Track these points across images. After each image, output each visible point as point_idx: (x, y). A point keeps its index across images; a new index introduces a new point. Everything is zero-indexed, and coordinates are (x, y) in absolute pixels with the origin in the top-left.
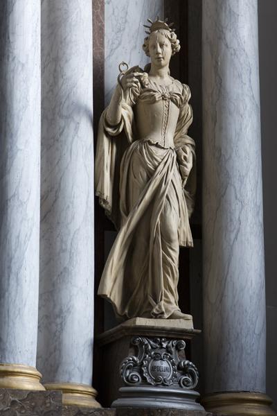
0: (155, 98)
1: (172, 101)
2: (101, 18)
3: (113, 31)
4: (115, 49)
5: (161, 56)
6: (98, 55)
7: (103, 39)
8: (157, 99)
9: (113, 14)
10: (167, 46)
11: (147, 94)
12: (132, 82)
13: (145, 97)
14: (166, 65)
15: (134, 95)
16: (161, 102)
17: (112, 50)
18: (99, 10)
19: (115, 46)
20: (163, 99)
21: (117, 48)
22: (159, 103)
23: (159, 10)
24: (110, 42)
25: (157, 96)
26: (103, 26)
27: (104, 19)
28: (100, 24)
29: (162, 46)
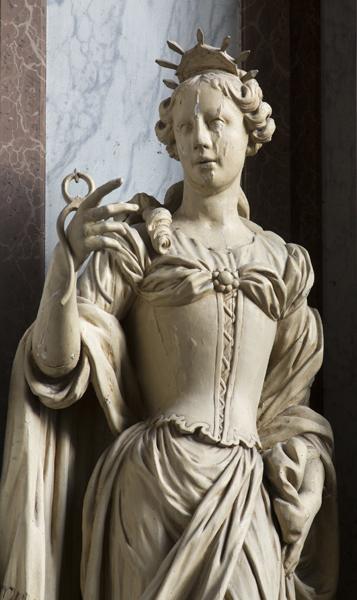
1: (248, 294)
3: (74, 87)
4: (82, 142)
5: (209, 154)
6: (24, 163)
7: (42, 110)
8: (196, 291)
10: (228, 122)
12: (105, 232)
13: (160, 284)
14: (229, 183)
15: (125, 279)
16: (211, 298)
18: (28, 24)
19: (79, 134)
20: (217, 289)
21: (88, 137)
22: (203, 302)
23: (223, 20)
24: (65, 124)
25: (198, 279)
26: (42, 71)
27: (42, 47)
28: (29, 67)
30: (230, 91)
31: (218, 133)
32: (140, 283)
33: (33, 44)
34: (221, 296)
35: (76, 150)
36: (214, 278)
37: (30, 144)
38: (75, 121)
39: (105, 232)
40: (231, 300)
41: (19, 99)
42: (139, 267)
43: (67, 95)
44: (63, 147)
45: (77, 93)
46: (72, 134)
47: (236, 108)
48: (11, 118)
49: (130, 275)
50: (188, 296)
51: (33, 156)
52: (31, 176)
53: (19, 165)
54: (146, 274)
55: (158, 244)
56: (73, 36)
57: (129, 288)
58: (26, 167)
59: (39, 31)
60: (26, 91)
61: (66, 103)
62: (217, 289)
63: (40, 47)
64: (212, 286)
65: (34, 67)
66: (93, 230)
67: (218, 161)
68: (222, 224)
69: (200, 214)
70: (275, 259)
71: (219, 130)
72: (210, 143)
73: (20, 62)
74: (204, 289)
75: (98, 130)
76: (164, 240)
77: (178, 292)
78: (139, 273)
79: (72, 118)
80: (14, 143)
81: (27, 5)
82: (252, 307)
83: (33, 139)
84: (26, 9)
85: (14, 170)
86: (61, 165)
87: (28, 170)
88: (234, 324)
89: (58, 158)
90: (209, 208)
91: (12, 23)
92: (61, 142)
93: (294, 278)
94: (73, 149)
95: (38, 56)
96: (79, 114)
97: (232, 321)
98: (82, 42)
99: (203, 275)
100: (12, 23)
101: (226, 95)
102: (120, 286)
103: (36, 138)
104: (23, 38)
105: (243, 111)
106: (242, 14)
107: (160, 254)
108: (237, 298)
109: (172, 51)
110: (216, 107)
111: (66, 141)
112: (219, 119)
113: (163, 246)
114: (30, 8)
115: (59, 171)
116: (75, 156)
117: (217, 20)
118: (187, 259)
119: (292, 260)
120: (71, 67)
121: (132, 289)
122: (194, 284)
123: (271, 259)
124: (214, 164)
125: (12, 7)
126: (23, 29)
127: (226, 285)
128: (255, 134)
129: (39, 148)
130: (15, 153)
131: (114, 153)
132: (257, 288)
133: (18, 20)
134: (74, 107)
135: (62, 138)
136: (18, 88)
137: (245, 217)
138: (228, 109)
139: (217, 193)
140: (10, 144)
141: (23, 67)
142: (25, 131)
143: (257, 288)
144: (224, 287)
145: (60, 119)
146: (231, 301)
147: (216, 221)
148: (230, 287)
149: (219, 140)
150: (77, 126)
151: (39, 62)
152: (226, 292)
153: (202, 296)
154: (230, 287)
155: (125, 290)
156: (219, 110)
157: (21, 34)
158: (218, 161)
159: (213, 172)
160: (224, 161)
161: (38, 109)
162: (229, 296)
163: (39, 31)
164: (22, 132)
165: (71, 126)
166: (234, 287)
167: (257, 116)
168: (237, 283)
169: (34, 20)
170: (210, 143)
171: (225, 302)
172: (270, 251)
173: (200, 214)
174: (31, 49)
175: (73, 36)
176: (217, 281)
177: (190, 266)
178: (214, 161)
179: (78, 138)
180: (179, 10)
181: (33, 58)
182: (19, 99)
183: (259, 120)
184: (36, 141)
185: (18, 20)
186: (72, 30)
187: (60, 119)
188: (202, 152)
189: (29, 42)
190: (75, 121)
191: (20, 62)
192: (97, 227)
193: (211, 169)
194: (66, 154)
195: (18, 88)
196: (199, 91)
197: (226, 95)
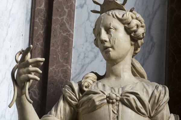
0: (94, 100)
1: (124, 103)
2: (68, 26)
3: (86, 41)
4: (89, 64)
5: (107, 44)
6: (60, 74)
7: (70, 52)
8: (97, 103)
9: (88, 19)
10: (116, 29)
11: (85, 98)
12: (30, 72)
13: (83, 103)
14: (123, 58)
15: (70, 104)
16: (106, 106)
17: (83, 66)
18: (65, 17)
19: (88, 60)
20: (108, 102)
21: (92, 61)
22: (102, 109)
23: (159, 6)
24: (81, 57)
25: (97, 99)
26: (72, 36)
27: (72, 26)
28: (65, 34)
29: (108, 30)
30: (116, 15)
31: (111, 34)
32: (77, 106)
33: (67, 25)
34: (111, 105)
35: (86, 67)
36: (107, 97)
37: (63, 66)
38: (86, 55)
39: (30, 72)
40: (116, 107)
41: (59, 48)
42: (76, 99)
43: (83, 45)
44: (81, 66)
45: (88, 44)
46: (85, 61)
47: (120, 23)
48: (55, 56)
49: (71, 102)
50: (94, 107)
51: (64, 71)
52: (63, 80)
53: (57, 75)
54: (79, 100)
55: (83, 86)
56: (87, 20)
57: (72, 108)
58: (60, 76)
59: (70, 19)
60: (63, 44)
61: (83, 48)
62: (108, 102)
63: (70, 26)
64: (106, 101)
65: (67, 34)
66: (23, 72)
67: (112, 47)
68: (121, 77)
69: (110, 74)
70: (147, 90)
71: (112, 33)
72: (108, 40)
73: (60, 33)
74: (102, 102)
75: (97, 58)
76: (86, 84)
77: (90, 105)
78: (76, 101)
79: (85, 54)
80: (56, 67)
81: (65, 9)
82: (130, 111)
83: (64, 64)
84: (65, 11)
85: (55, 78)
86: (79, 74)
87: (62, 77)
88: (117, 117)
89: (78, 71)
90: (114, 71)
91: (58, 17)
92: (79, 65)
93: (154, 97)
94: (85, 67)
95: (69, 29)
96: (88, 52)
97: (116, 116)
98: (91, 22)
99: (101, 96)
100: (58, 17)
101: (114, 17)
102: (68, 108)
103: (66, 63)
104: (62, 23)
105: (124, 24)
106: (168, 2)
107: (85, 91)
108: (118, 105)
109: (96, 4)
110: (109, 23)
111: (81, 64)
112: (111, 28)
113: (86, 87)
114: (67, 10)
115: (77, 77)
116: (85, 70)
117: (156, 6)
118: (94, 90)
119: (155, 91)
120: (86, 33)
121: (74, 108)
122: (96, 100)
123: (145, 90)
124: (111, 49)
125: (58, 11)
126: (63, 19)
127: (112, 99)
128: (132, 35)
129: (67, 68)
130: (56, 71)
131: (38, 40)
132: (127, 100)
133: (60, 16)
134: (86, 49)
135: (80, 63)
136: (59, 44)
137: (144, 78)
138: (115, 23)
139: (117, 63)
140: (54, 67)
141: (62, 35)
142: (61, 61)
143: (127, 100)
144: (111, 101)
145: (79, 55)
146: (116, 107)
147: (118, 76)
148: (115, 101)
149: (112, 37)
150: (87, 57)
151: (69, 32)
152: (113, 103)
153: (101, 106)
154: (115, 101)
155: (71, 109)
156: (110, 24)
157: (61, 21)
158: (112, 47)
159: (110, 53)
160: (115, 47)
161: (68, 51)
162: (114, 105)
163: (70, 19)
164: (60, 61)
165: (84, 57)
166: (117, 101)
167: (129, 25)
168: (118, 99)
169: (68, 15)
170: (108, 40)
171: (113, 107)
172: (145, 87)
173: (110, 74)
174: (66, 27)
175: (87, 20)
176: (108, 99)
177: (95, 93)
178: (111, 48)
179: (88, 62)
180: (138, 4)
181: (67, 31)
182: (59, 48)
183: (131, 27)
184: (66, 65)
185: (60, 16)
186: (87, 17)
187: (79, 55)
188: (104, 44)
189: (65, 24)
190: (86, 55)
191: (60, 33)
192: (25, 70)
193: (109, 51)
194: (82, 69)
195: (59, 44)
196: (103, 18)
197: (114, 17)
